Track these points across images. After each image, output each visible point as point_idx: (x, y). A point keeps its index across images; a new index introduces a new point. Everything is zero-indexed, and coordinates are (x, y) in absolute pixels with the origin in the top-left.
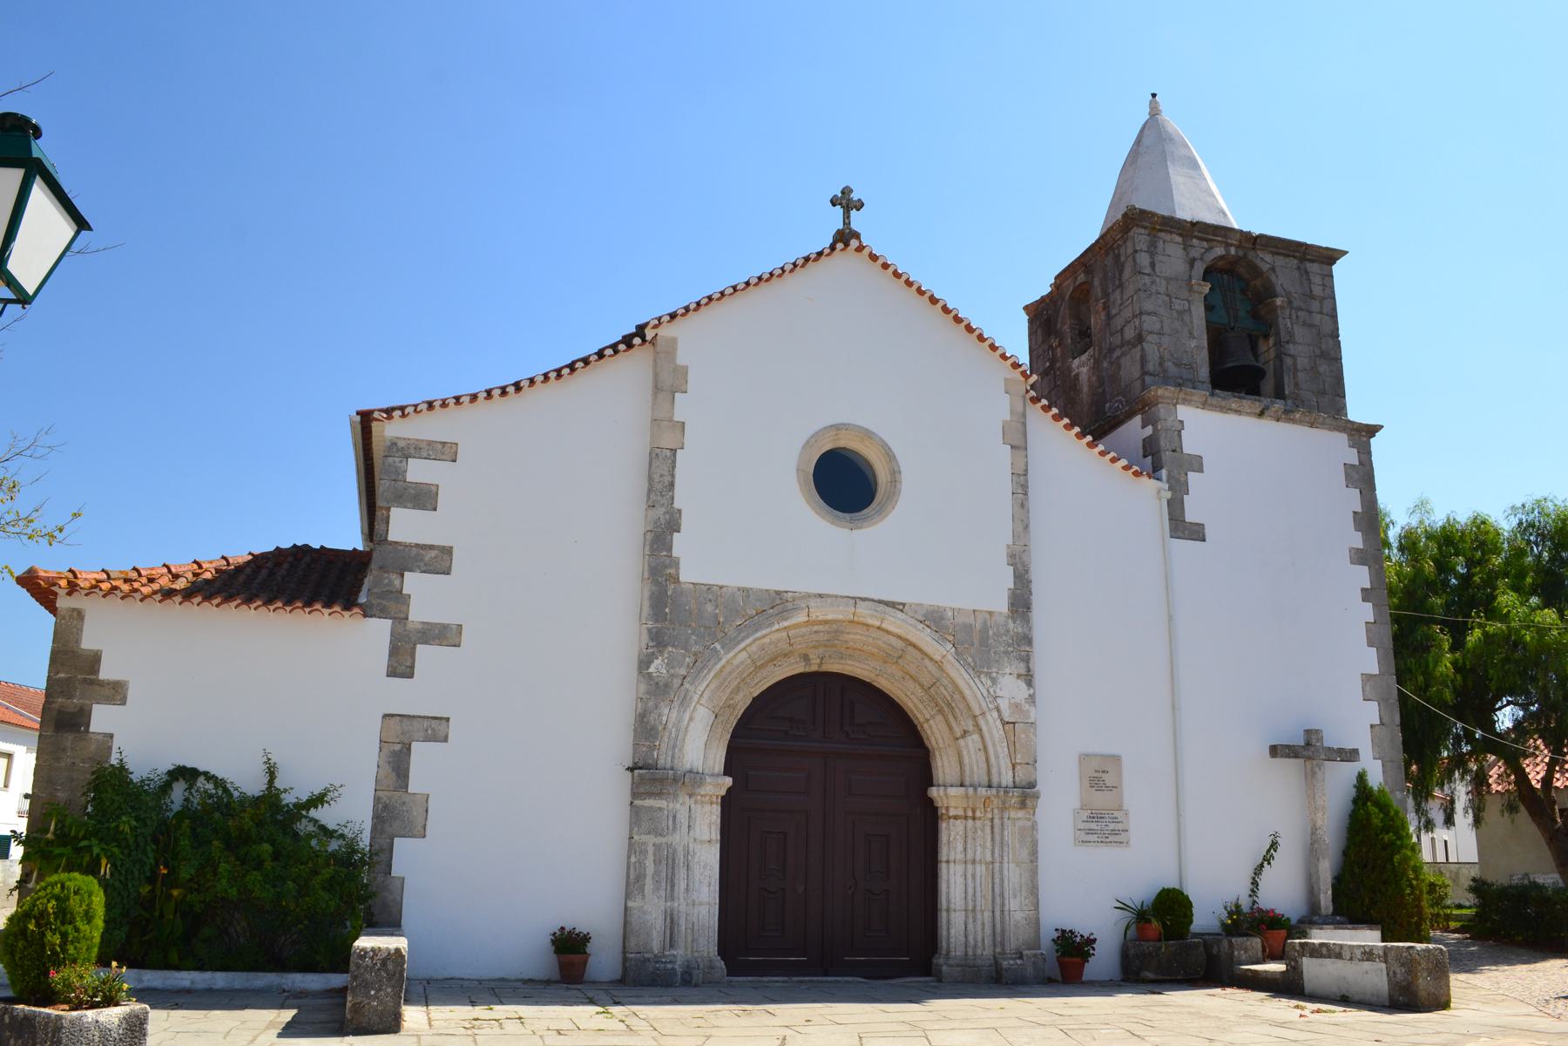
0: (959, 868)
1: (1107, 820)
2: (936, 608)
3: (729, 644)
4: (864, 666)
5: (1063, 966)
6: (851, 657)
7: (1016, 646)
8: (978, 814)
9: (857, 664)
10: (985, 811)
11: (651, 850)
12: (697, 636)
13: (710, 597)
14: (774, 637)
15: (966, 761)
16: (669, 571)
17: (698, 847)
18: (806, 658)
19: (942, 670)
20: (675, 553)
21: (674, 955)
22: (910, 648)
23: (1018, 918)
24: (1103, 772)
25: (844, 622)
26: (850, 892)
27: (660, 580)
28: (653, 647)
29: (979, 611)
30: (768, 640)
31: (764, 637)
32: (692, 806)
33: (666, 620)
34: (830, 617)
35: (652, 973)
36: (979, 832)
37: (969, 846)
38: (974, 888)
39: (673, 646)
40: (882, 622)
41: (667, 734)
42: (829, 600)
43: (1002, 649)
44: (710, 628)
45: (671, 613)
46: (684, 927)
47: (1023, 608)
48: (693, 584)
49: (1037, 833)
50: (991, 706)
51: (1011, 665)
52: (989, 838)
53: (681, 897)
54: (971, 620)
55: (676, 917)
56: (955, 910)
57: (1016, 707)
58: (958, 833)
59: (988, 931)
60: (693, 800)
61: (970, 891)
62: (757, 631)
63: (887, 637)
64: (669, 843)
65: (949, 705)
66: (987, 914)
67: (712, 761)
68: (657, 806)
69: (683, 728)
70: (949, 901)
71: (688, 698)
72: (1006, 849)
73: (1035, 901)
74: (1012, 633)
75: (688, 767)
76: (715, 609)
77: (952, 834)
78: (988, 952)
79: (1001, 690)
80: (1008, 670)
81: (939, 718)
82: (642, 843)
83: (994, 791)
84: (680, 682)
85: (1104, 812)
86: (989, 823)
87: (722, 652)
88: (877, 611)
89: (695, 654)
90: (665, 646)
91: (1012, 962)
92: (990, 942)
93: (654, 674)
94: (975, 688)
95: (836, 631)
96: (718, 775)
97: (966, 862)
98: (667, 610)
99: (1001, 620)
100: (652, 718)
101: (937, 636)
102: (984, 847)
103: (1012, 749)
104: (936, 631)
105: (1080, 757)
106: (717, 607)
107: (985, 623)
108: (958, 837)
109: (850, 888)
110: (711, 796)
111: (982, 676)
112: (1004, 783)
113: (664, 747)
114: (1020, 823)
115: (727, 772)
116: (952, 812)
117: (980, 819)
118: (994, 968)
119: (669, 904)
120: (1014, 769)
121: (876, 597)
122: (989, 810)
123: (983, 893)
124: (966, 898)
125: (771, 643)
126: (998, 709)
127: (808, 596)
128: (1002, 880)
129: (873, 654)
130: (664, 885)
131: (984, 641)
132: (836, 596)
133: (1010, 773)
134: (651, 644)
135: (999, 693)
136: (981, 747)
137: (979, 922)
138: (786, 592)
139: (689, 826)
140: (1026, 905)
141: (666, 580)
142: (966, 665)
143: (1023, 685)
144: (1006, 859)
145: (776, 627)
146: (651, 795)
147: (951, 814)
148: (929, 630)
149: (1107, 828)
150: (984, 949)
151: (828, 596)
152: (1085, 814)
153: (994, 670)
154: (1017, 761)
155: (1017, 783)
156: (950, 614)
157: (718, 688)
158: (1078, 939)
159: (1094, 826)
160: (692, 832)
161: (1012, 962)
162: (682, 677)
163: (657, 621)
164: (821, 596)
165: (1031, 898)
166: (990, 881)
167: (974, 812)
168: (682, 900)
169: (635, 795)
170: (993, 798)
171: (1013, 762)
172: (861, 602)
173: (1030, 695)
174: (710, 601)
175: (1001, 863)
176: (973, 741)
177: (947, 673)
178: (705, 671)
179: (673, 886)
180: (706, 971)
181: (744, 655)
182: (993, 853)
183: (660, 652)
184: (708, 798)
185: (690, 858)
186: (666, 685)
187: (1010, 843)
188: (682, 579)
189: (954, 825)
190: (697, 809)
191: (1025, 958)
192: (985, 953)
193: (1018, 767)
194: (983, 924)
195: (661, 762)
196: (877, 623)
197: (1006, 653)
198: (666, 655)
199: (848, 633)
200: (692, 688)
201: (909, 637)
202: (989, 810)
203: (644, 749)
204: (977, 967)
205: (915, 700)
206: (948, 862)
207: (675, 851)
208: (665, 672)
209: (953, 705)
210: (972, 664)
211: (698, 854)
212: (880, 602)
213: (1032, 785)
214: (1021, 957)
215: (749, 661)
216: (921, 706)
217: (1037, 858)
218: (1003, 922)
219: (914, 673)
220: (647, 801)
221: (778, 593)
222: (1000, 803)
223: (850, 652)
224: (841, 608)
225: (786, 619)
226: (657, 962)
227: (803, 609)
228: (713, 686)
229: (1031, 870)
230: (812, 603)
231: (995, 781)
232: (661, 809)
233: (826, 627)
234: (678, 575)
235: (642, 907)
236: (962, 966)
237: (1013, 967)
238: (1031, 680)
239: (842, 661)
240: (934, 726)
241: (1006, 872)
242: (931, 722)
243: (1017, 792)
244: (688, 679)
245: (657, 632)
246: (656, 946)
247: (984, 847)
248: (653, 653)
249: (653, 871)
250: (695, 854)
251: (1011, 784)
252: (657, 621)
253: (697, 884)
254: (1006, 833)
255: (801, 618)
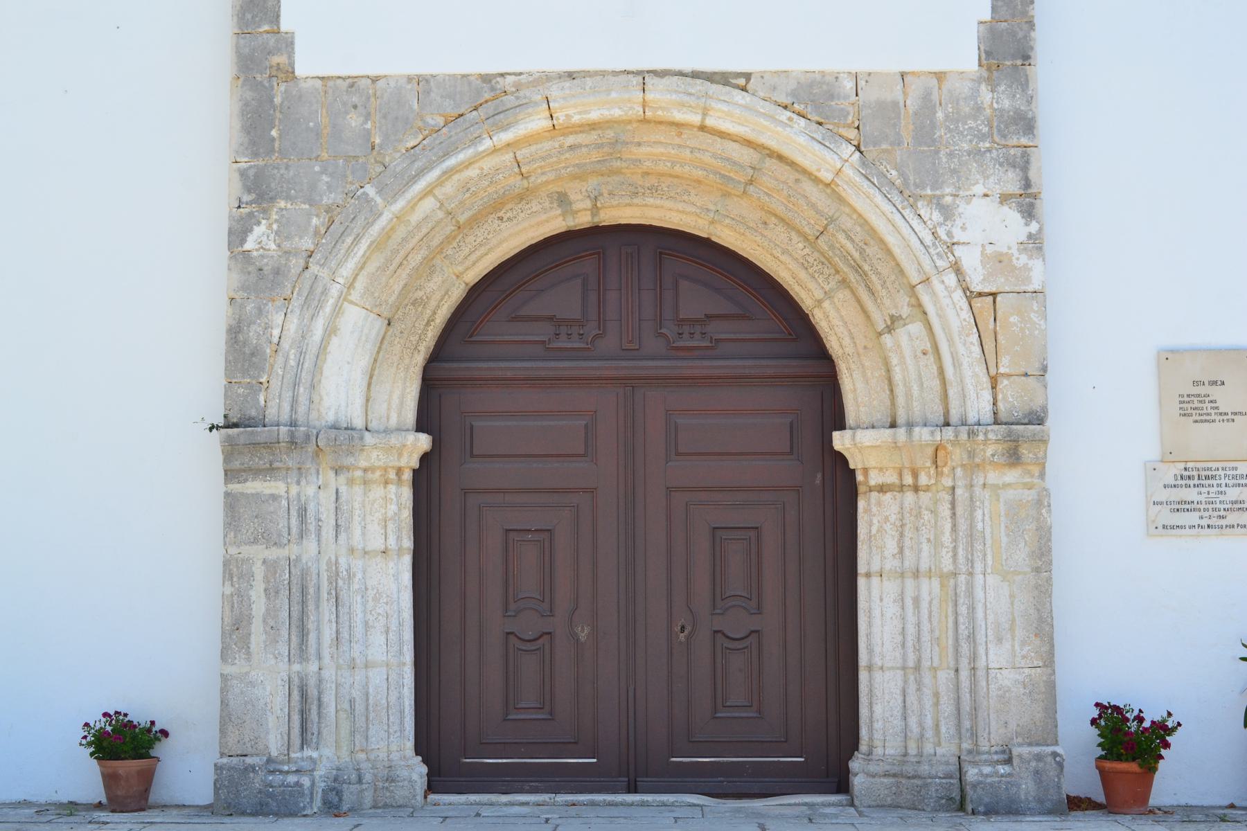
0: (890, 587)
1: (1223, 482)
2: (818, 77)
3: (393, 187)
4: (680, 206)
5: (1106, 778)
6: (653, 190)
7: (997, 139)
8: (923, 480)
9: (668, 204)
10: (939, 474)
11: (259, 571)
12: (331, 175)
13: (355, 99)
14: (488, 164)
15: (898, 376)
16: (275, 60)
17: (357, 565)
18: (562, 200)
19: (841, 200)
20: (285, 26)
21: (311, 758)
22: (771, 164)
23: (1007, 683)
24: (1214, 383)
25: (630, 122)
26: (682, 637)
27: (259, 78)
28: (250, 203)
29: (913, 73)
30: (478, 171)
31: (468, 164)
32: (343, 489)
33: (272, 151)
34: (594, 115)
35: (260, 792)
36: (926, 515)
37: (907, 543)
38: (919, 625)
39: (288, 198)
40: (705, 115)
41: (280, 360)
42: (589, 82)
43: (966, 146)
44: (356, 157)
45: (281, 136)
46: (332, 709)
47: (1014, 57)
48: (322, 78)
49: (1049, 511)
50: (941, 264)
51: (987, 177)
52: (948, 526)
53: (326, 653)
54: (897, 93)
55: (312, 692)
56: (882, 668)
57: (1000, 261)
58: (887, 519)
59: (947, 707)
60: (342, 479)
61: (911, 630)
62: (446, 155)
63: (718, 145)
64: (293, 557)
65: (857, 269)
66: (944, 676)
67: (385, 406)
68: (267, 492)
69: (313, 349)
70: (871, 651)
71: (319, 290)
72: (979, 547)
73: (1045, 648)
74: (988, 111)
75: (330, 417)
76: (365, 122)
77: (875, 521)
78: (947, 749)
79: (963, 228)
80: (979, 189)
81: (842, 295)
82: (243, 560)
83: (949, 433)
84: (302, 263)
85: (1214, 465)
86: (948, 497)
87: (379, 200)
88: (690, 94)
89: (328, 210)
90: (273, 199)
91: (987, 770)
92: (953, 731)
93: (255, 254)
94: (906, 231)
95: (615, 143)
96: (408, 430)
97: (902, 575)
98: (274, 133)
99: (964, 88)
100: (253, 333)
101: (819, 133)
102: (936, 543)
103: (989, 346)
104: (820, 124)
105: (1158, 352)
106: (368, 117)
107: (926, 97)
108: (888, 527)
109: (683, 629)
110: (385, 469)
111: (920, 204)
112: (972, 417)
113: (276, 384)
114: (1010, 494)
115: (421, 427)
116: (875, 479)
117: (927, 489)
118: (955, 781)
119: (296, 667)
120: (994, 388)
121: (687, 67)
122: (946, 470)
123: (937, 634)
124: (903, 645)
125: (482, 176)
126: (957, 269)
127: (547, 78)
128: (972, 609)
129: (699, 182)
130: (285, 633)
131: (925, 133)
132: (603, 74)
133: (987, 396)
134: (246, 198)
135: (958, 235)
136: (928, 346)
137: (927, 692)
138: (502, 75)
139: (337, 525)
140: (1024, 657)
141: (271, 77)
142: (884, 185)
143: (1013, 216)
144: (979, 567)
145: (487, 144)
146: (257, 473)
147: (872, 483)
148: (802, 122)
149: (1222, 498)
150: (939, 744)
151: (587, 74)
152: (1170, 472)
153: (948, 190)
154: (1002, 370)
155: (1003, 416)
156: (849, 85)
157: (382, 268)
158: (1133, 726)
159: (1191, 494)
160: (343, 537)
161: (987, 770)
162: (305, 255)
163: (255, 155)
164: (571, 75)
165: (1037, 642)
166: (950, 610)
167: (915, 475)
168: (327, 659)
169: (230, 475)
170: (950, 448)
171: (993, 372)
172: (656, 80)
173: (1030, 236)
174: (355, 107)
175: (971, 574)
176: (910, 336)
177: (850, 205)
178: (349, 240)
179: (303, 634)
180: (381, 784)
181: (429, 204)
182: (955, 556)
183: (265, 211)
184: (378, 473)
185: (340, 583)
186: (277, 272)
187: (988, 535)
188: (300, 71)
189: (879, 504)
190: (355, 496)
191: (1016, 761)
192: (940, 751)
193: (1003, 383)
194: (936, 695)
195: (271, 414)
196: (696, 119)
197: (976, 153)
198: (275, 217)
199: (639, 144)
200: (324, 274)
201: (763, 140)
202: (946, 470)
203: (241, 391)
204: (919, 777)
205: (793, 266)
206: (868, 575)
207: (304, 575)
208: (273, 247)
209: (866, 268)
210: (898, 182)
211: (359, 576)
212: (695, 75)
213: (1037, 418)
214: (1009, 761)
215: (440, 214)
216: (803, 275)
217: (1050, 563)
218: (973, 691)
219: (780, 210)
220: (249, 484)
221: (486, 78)
222: (965, 456)
223: (653, 180)
224: (614, 95)
225: (505, 128)
226: (272, 772)
227: (536, 104)
228: (371, 267)
229: (1037, 587)
230: (555, 91)
231: (954, 417)
232: (274, 497)
233: (593, 136)
234: (292, 65)
235: (247, 673)
236: (895, 775)
237: (989, 780)
238: (1032, 205)
239: (636, 201)
240: (832, 314)
241: (979, 594)
242: (826, 304)
243: (996, 432)
244: (317, 256)
245: (256, 176)
246: (274, 745)
247: (936, 543)
248: (251, 215)
249: (263, 609)
250: (350, 576)
251: (987, 417)
252: (255, 155)
253: (359, 629)
254: (979, 514)
255: (536, 122)
